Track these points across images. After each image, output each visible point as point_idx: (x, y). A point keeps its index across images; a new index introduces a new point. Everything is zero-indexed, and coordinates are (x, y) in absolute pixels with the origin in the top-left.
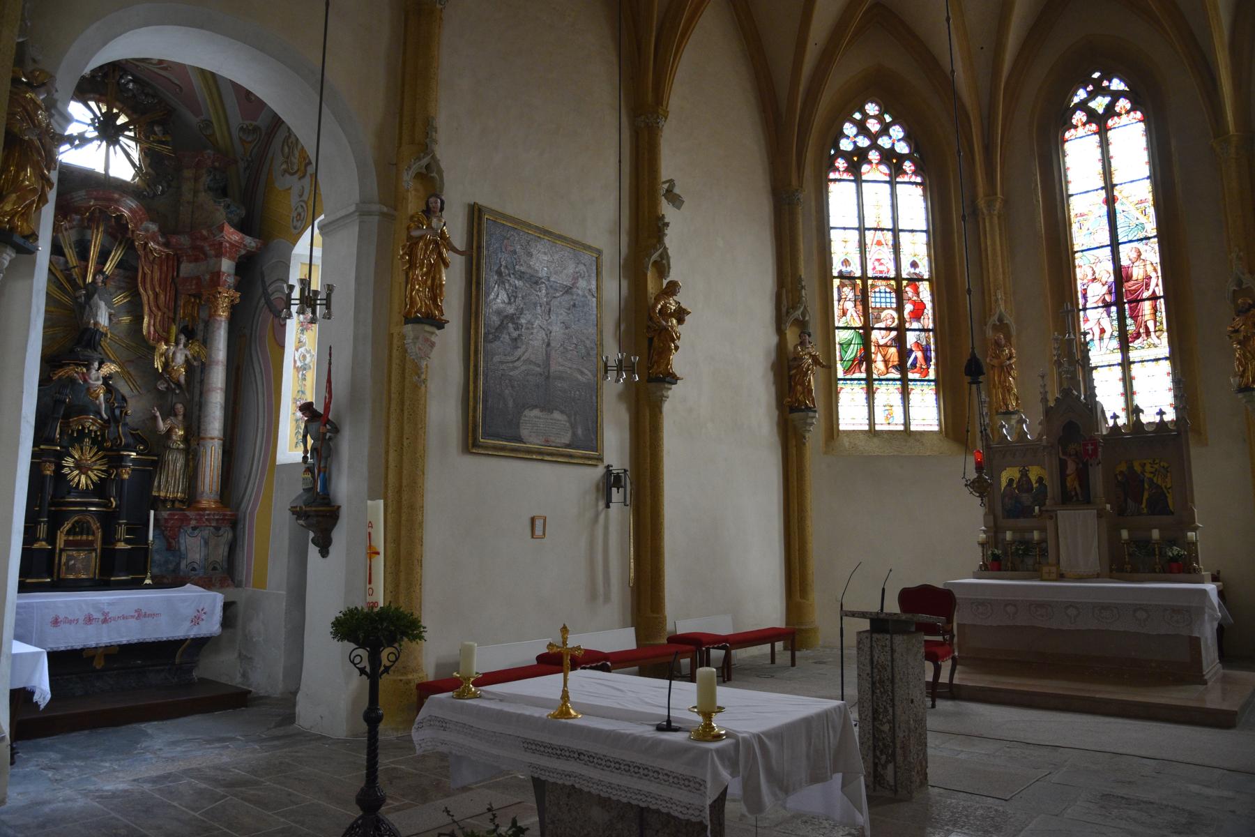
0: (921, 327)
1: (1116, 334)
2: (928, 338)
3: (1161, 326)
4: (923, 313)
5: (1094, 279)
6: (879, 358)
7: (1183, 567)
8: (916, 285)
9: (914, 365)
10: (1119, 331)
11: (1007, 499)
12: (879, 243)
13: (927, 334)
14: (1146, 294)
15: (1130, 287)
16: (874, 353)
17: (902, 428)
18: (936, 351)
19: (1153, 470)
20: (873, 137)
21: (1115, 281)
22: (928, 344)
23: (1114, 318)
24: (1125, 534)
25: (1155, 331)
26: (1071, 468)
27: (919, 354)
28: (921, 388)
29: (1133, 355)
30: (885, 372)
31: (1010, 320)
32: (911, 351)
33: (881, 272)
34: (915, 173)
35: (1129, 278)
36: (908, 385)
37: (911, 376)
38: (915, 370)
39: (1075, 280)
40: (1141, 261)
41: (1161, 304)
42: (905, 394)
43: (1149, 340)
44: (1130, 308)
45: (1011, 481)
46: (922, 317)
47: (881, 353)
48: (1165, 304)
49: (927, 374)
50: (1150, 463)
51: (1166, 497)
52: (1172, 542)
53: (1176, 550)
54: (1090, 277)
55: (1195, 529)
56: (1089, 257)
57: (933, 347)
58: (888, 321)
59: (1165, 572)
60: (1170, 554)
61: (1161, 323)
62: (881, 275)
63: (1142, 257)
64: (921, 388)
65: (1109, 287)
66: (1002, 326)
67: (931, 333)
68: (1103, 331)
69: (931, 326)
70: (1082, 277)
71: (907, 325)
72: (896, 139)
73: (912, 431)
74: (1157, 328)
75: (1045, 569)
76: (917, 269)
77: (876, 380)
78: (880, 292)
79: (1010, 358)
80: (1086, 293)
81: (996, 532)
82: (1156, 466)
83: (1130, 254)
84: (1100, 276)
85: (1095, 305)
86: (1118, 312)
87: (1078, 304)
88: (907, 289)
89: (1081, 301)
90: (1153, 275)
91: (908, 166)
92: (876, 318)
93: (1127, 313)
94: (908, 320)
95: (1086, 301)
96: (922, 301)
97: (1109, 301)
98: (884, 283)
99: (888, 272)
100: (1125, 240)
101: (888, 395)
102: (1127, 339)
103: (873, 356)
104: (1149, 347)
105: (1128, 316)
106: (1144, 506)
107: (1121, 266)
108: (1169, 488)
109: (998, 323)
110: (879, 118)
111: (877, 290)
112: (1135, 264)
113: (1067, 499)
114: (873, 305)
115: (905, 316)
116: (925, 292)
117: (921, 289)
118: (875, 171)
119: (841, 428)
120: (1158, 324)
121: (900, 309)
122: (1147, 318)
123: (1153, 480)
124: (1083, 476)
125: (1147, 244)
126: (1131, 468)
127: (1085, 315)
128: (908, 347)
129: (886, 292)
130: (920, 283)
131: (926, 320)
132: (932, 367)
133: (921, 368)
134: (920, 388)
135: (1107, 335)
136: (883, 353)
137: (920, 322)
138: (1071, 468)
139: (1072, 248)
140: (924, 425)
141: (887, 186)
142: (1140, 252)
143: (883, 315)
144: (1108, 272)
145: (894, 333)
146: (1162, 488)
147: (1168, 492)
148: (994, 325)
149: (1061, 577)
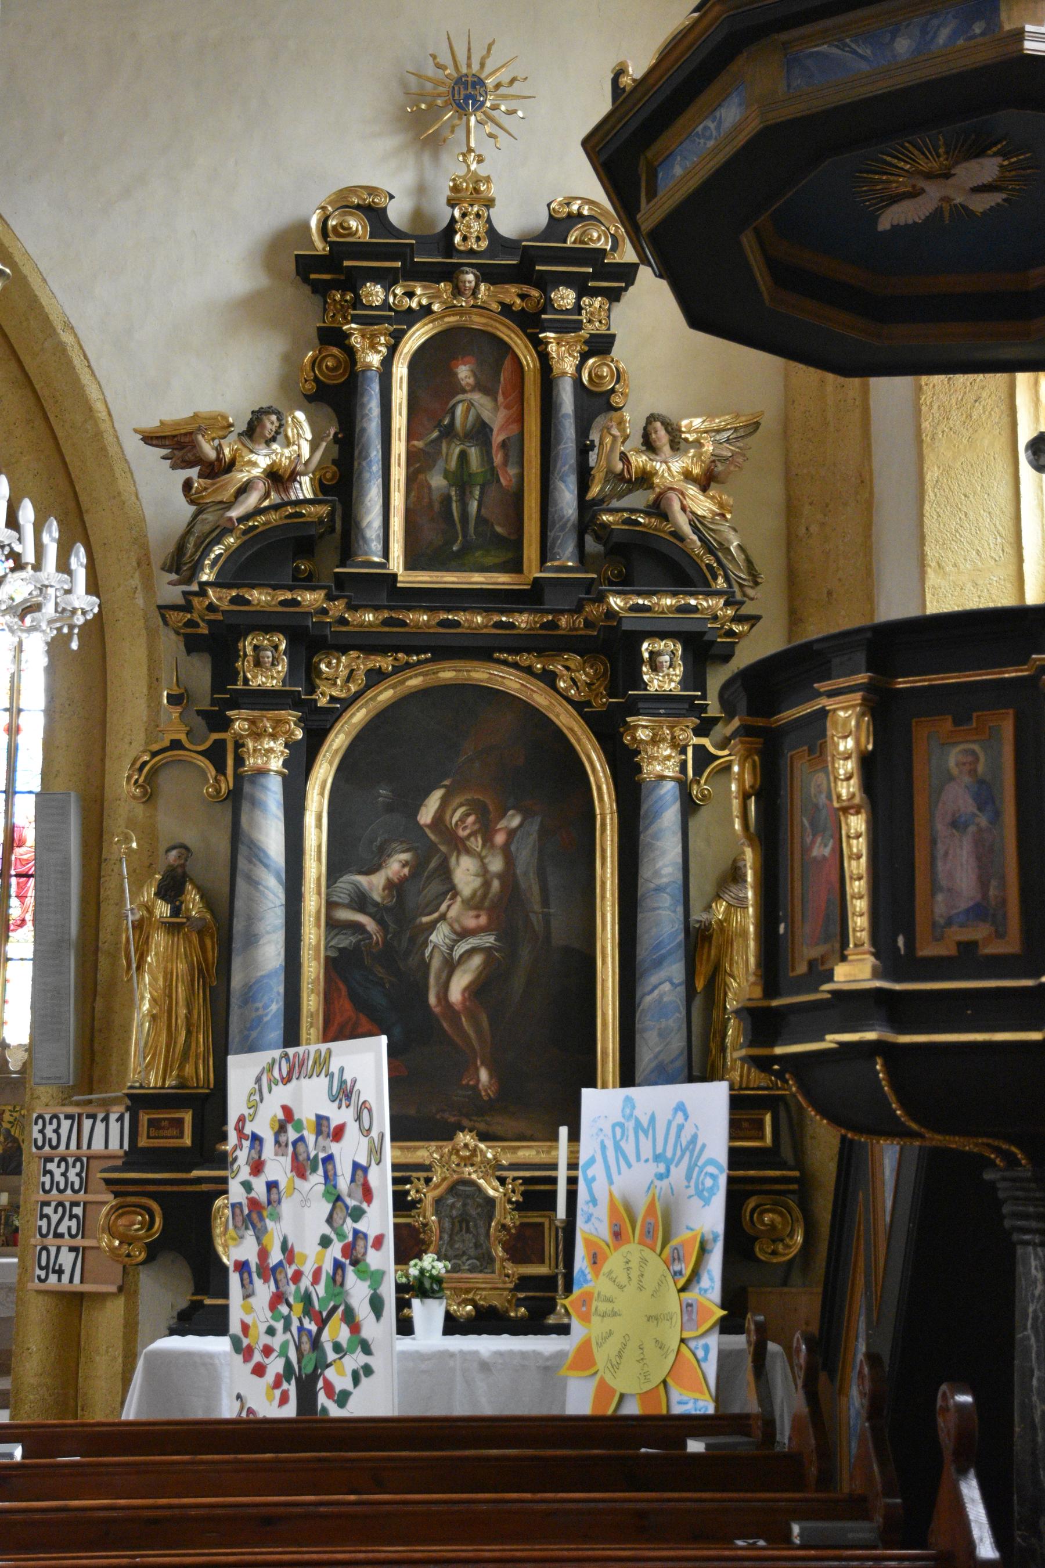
19: (12, 1119)
44: (18, 883)
59: (8, 1245)
82: (15, 1114)
119: (711, 1410)
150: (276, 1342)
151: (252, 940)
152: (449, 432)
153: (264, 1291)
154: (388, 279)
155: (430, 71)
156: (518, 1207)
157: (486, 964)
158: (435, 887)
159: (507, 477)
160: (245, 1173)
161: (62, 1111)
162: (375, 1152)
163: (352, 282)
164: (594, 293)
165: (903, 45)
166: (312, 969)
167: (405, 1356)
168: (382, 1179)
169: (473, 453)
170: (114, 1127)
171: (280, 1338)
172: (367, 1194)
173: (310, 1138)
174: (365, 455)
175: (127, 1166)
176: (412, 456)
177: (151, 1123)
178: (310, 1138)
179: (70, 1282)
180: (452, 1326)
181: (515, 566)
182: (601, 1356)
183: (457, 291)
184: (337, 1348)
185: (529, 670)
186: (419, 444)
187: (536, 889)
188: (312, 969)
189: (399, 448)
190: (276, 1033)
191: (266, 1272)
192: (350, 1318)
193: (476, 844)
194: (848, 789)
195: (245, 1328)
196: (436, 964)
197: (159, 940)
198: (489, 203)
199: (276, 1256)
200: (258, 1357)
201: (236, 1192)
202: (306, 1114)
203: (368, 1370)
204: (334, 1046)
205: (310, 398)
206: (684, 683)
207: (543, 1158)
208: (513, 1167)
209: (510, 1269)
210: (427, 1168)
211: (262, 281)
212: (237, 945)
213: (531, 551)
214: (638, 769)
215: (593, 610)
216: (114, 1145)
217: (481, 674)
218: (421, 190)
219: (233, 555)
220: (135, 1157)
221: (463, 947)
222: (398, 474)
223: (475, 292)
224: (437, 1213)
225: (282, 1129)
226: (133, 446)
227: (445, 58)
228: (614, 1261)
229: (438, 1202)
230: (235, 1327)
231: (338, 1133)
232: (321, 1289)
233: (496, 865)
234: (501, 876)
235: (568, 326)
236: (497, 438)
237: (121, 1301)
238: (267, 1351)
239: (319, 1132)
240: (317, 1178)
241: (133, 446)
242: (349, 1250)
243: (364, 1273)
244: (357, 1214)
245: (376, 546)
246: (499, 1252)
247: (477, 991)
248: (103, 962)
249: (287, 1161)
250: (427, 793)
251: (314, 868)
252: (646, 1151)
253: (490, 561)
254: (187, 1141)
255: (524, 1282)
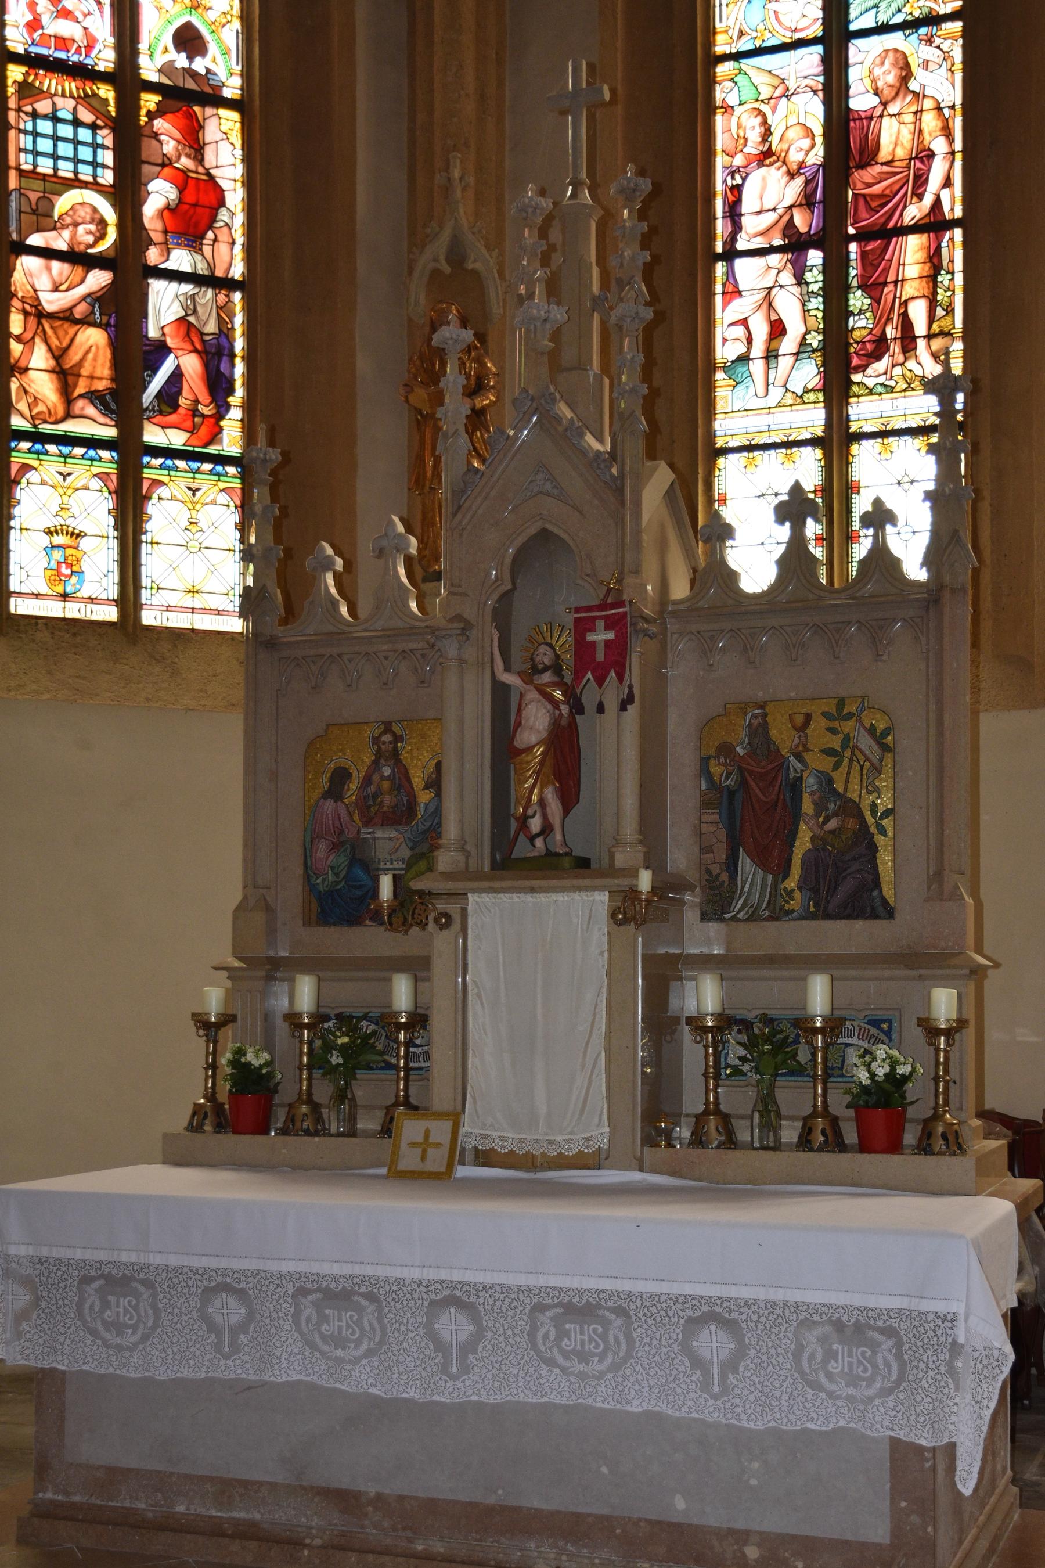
0: (202, 269)
1: (815, 340)
2: (224, 312)
3: (949, 319)
4: (213, 219)
5: (766, 157)
6: (40, 358)
8: (192, 117)
10: (824, 332)
11: (321, 850)
13: (222, 298)
14: (913, 212)
15: (869, 185)
16: (18, 339)
17: (110, 614)
18: (250, 359)
21: (827, 164)
22: (225, 333)
23: (815, 288)
25: (929, 337)
27: (191, 364)
28: (189, 482)
30: (61, 412)
32: (161, 350)
33: (62, 43)
35: (869, 154)
36: (142, 466)
37: (153, 435)
38: (173, 418)
39: (710, 153)
40: (909, 98)
43: (911, 364)
44: (863, 255)
46: (210, 235)
47: (46, 341)
48: (965, 244)
49: (215, 435)
50: (825, 715)
51: (873, 848)
54: (753, 148)
56: (760, 79)
57: (239, 344)
58: (81, 229)
60: (863, 1076)
61: (950, 310)
62: (61, 55)
63: (913, 86)
64: (189, 482)
65: (807, 182)
67: (237, 296)
68: (777, 329)
69: (238, 271)
70: (730, 146)
71: (153, 256)
73: (149, 629)
74: (935, 327)
76: (198, 60)
77: (21, 435)
78: (55, 119)
80: (738, 201)
83: (878, 72)
84: (785, 146)
85: (759, 243)
86: (827, 268)
87: (711, 237)
88: (159, 124)
89: (721, 227)
90: (939, 146)
92: (34, 212)
93: (853, 273)
94: (157, 237)
95: (737, 227)
96: (212, 178)
97: (803, 229)
98: (71, 86)
99: (89, 48)
100: (867, 22)
102: (849, 361)
103: (16, 348)
104: (909, 388)
105: (855, 283)
106: (791, 883)
107: (848, 109)
108: (887, 813)
109: (447, 269)
111: (43, 106)
112: (893, 109)
114: (26, 162)
115: (147, 223)
116: (224, 146)
117: (211, 132)
120: (940, 312)
122: (909, 290)
123: (830, 781)
125: (929, 41)
127: (730, 273)
128: (153, 333)
129: (76, 123)
130: (209, 111)
131: (223, 248)
132: (236, 413)
133: (194, 412)
134: (187, 480)
135: (788, 344)
136: (54, 342)
137: (200, 251)
139: (709, 43)
140: (193, 610)
142: (907, 66)
143: (64, 203)
144: (809, 133)
145: (98, 279)
146: (860, 815)
147: (883, 831)
148: (436, 273)
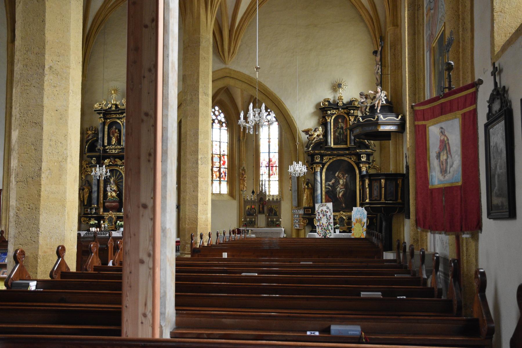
2: (226, 170)
7: (279, 225)
9: (222, 177)
12: (216, 145)
20: (216, 116)
22: (226, 172)
24: (270, 219)
26: (261, 206)
29: (271, 179)
31: (245, 168)
34: (226, 127)
41: (277, 168)
42: (220, 183)
45: (248, 208)
52: (277, 221)
53: (278, 222)
55: (281, 219)
66: (244, 170)
68: (265, 173)
72: (222, 117)
75: (255, 226)
79: (245, 178)
81: (245, 219)
91: (224, 125)
101: (216, 184)
110: (218, 111)
113: (260, 212)
118: (216, 125)
121: (220, 162)
124: (263, 208)
126: (271, 207)
138: (261, 206)
141: (219, 130)
145: (218, 169)
149: (258, 228)
150: (322, 233)
151: (317, 190)
152: (338, 128)
153: (320, 228)
154: (330, 110)
155: (335, 83)
156: (347, 220)
157: (344, 192)
158: (338, 183)
159: (345, 134)
160: (318, 216)
161: (296, 209)
162: (331, 214)
163: (327, 111)
164: (356, 110)
165: (370, 128)
166: (324, 193)
167: (335, 235)
168: (332, 217)
169: (341, 130)
170: (302, 211)
171: (322, 232)
172: (330, 218)
173: (325, 213)
174: (328, 132)
175: (304, 215)
176: (334, 131)
177: (306, 211)
178: (325, 213)
179: (298, 228)
180: (340, 232)
181: (346, 144)
182: (355, 234)
183: (339, 111)
184: (328, 233)
185: (348, 157)
186: (335, 130)
187: (349, 183)
188: (324, 193)
189: (332, 130)
190: (320, 201)
191: (320, 226)
192: (329, 230)
193: (342, 178)
194: (367, 186)
195: (318, 232)
196: (338, 192)
197: (306, 190)
198: (342, 99)
199: (321, 224)
200: (320, 234)
201: (317, 218)
202: (324, 210)
203: (331, 235)
204: (327, 203)
205: (321, 125)
206: (366, 160)
207: (350, 214)
208: (347, 215)
209: (347, 226)
210: (337, 215)
211: (315, 110)
212: (315, 191)
213: (348, 142)
214: (361, 170)
215: (356, 151)
216: (302, 213)
217: (342, 158)
218: (334, 97)
219: (313, 146)
220: (305, 214)
221: (341, 190)
222: (332, 134)
223: (341, 111)
224: (338, 220)
225: (321, 211)
226: (301, 132)
227: (337, 81)
228: (356, 225)
229: (338, 219)
230: (317, 232)
231: (327, 212)
232: (326, 227)
233: (345, 181)
234: (345, 182)
235: (352, 115)
236: (344, 129)
237: (304, 230)
238: (321, 234)
239: (325, 212)
240: (325, 216)
241: (301, 132)
242: (329, 224)
243: (330, 226)
244: (330, 220)
245: (330, 143)
246: (345, 224)
247: (342, 195)
248: (299, 192)
249: (322, 215)
250: (336, 173)
251: (323, 182)
252: (359, 214)
253: (343, 144)
254: (310, 212)
255: (348, 228)
